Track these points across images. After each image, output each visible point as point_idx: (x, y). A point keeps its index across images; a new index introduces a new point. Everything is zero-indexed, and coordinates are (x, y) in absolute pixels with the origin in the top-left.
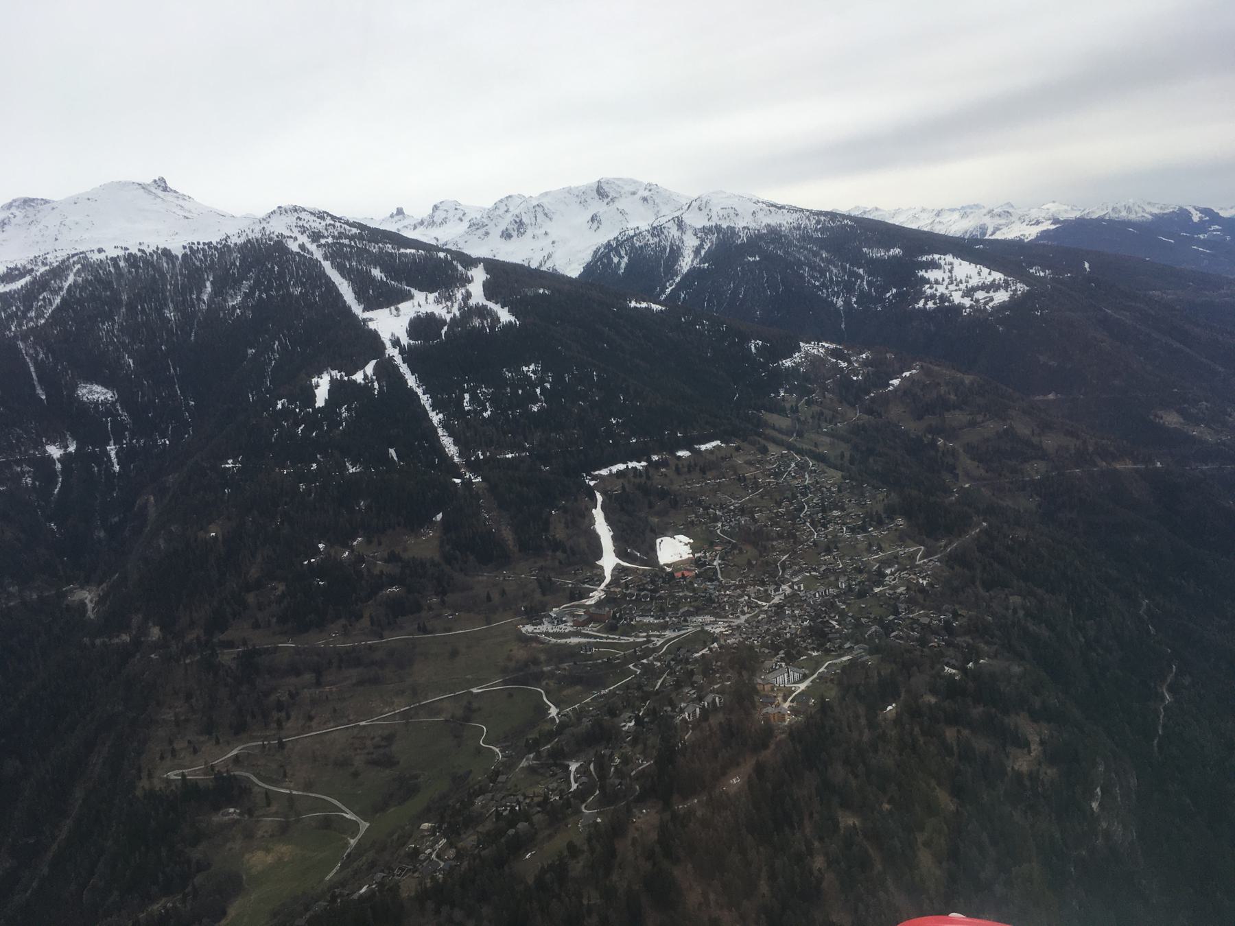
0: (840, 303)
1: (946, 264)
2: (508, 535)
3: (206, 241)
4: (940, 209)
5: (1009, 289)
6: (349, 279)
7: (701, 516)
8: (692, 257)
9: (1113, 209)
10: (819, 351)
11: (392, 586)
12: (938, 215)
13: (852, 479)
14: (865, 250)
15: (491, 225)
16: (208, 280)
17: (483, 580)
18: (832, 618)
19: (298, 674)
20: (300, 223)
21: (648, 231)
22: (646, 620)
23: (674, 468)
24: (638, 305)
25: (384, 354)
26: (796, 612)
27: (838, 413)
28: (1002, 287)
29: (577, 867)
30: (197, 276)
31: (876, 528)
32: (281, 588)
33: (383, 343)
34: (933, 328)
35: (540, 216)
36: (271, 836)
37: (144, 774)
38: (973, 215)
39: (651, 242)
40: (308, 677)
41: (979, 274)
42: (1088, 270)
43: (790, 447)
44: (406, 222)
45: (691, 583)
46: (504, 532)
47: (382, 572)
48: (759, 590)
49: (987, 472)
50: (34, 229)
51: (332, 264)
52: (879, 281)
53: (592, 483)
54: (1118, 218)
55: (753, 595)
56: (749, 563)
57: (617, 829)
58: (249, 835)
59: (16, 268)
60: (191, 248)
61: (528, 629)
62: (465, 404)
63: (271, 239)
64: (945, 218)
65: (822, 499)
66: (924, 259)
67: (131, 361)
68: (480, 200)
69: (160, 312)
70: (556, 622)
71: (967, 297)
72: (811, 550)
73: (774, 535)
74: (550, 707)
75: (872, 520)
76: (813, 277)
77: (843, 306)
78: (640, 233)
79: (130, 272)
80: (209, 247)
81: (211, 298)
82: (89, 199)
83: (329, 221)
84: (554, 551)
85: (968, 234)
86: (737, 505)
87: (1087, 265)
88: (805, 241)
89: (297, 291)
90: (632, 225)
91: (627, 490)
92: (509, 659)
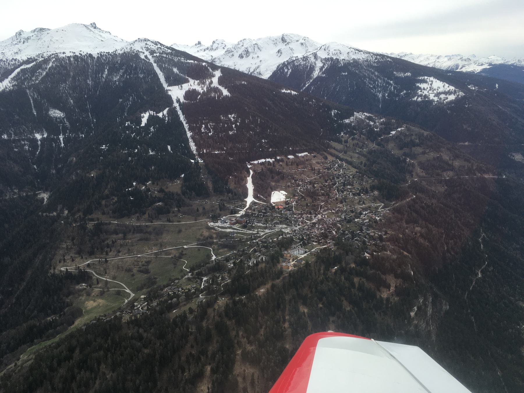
0: (380, 95)
1: (429, 81)
2: (210, 185)
3: (107, 52)
4: (439, 56)
5: (456, 94)
6: (163, 72)
7: (293, 184)
8: (319, 71)
9: (518, 61)
10: (362, 117)
11: (159, 202)
12: (438, 58)
13: (360, 173)
14: (395, 72)
15: (235, 51)
16: (106, 68)
17: (197, 203)
18: (333, 230)
19: (117, 234)
20: (147, 46)
21: (301, 58)
22: (259, 224)
23: (285, 163)
24: (286, 92)
25: (172, 105)
26: (320, 226)
27: (365, 144)
28: (453, 93)
29: (190, 317)
30: (102, 66)
31: (364, 194)
32: (116, 199)
33: (172, 101)
34: (419, 110)
35: (256, 49)
36: (97, 296)
37: (52, 267)
38: (454, 59)
39: (302, 63)
40: (121, 235)
41: (444, 86)
42: (497, 88)
43: (337, 157)
44: (201, 48)
45: (281, 211)
46: (209, 184)
47: (156, 196)
48: (308, 216)
49: (426, 174)
50: (40, 42)
51: (157, 65)
52: (399, 87)
53: (249, 167)
54: (520, 65)
55: (305, 218)
56: (307, 204)
57: (210, 304)
58: (88, 294)
59: (31, 58)
60: (101, 54)
61: (211, 224)
62: (202, 129)
63: (133, 52)
64: (441, 60)
65: (345, 181)
66: (420, 78)
67: (72, 101)
68: (231, 41)
69: (85, 81)
70: (223, 222)
71: (436, 96)
72: (334, 202)
73: (320, 194)
74: (213, 256)
75: (363, 191)
76: (370, 83)
77: (382, 97)
78: (298, 59)
79: (75, 63)
80: (108, 54)
81: (107, 77)
82: (63, 30)
83: (159, 46)
84: (228, 193)
85: (450, 68)
86: (308, 180)
87: (497, 85)
88: (369, 66)
89: (141, 76)
90: (295, 55)
91: (264, 171)
92: (201, 235)
